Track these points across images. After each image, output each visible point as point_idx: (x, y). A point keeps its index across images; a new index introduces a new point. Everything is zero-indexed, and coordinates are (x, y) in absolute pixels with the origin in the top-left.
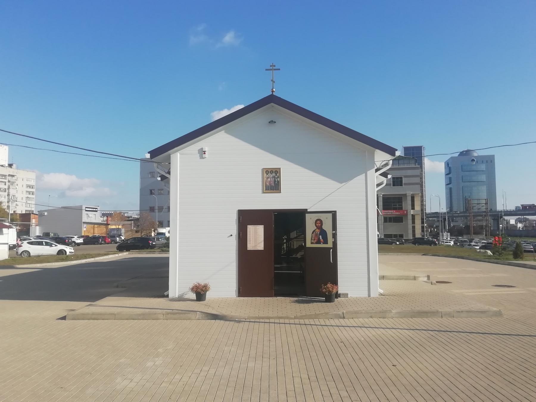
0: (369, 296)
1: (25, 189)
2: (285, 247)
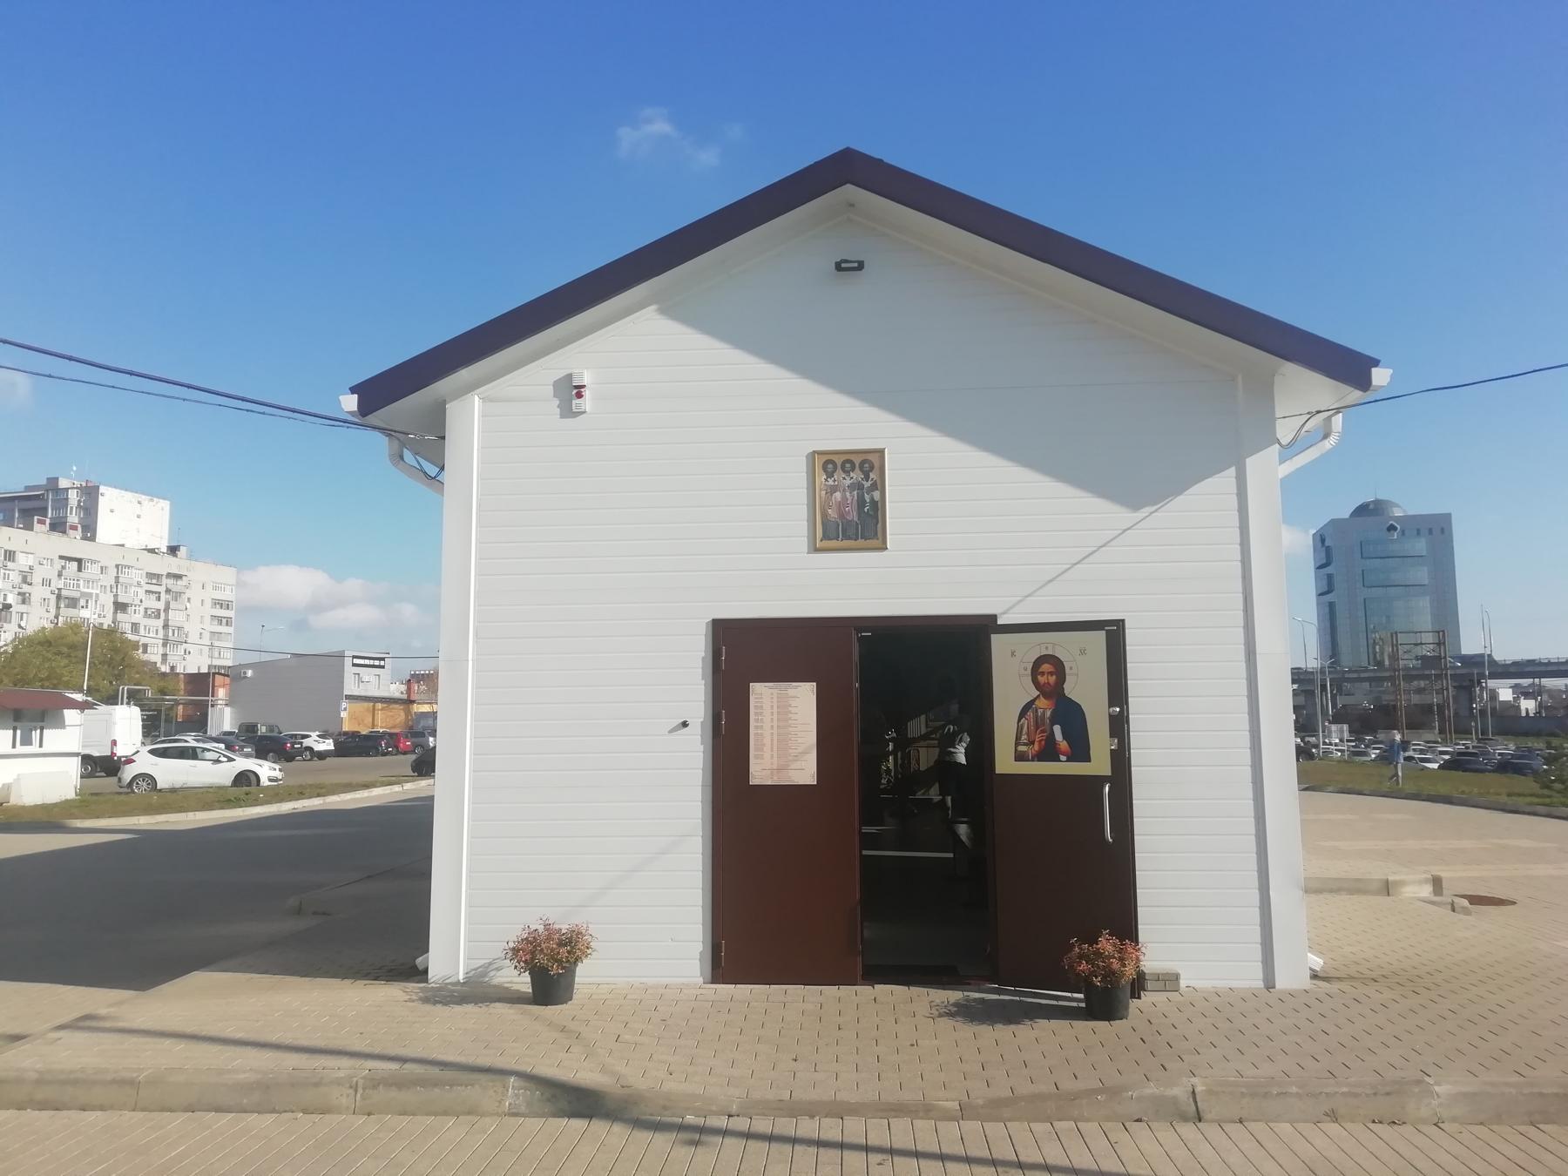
0: (1270, 984)
1: (210, 611)
2: (891, 765)
